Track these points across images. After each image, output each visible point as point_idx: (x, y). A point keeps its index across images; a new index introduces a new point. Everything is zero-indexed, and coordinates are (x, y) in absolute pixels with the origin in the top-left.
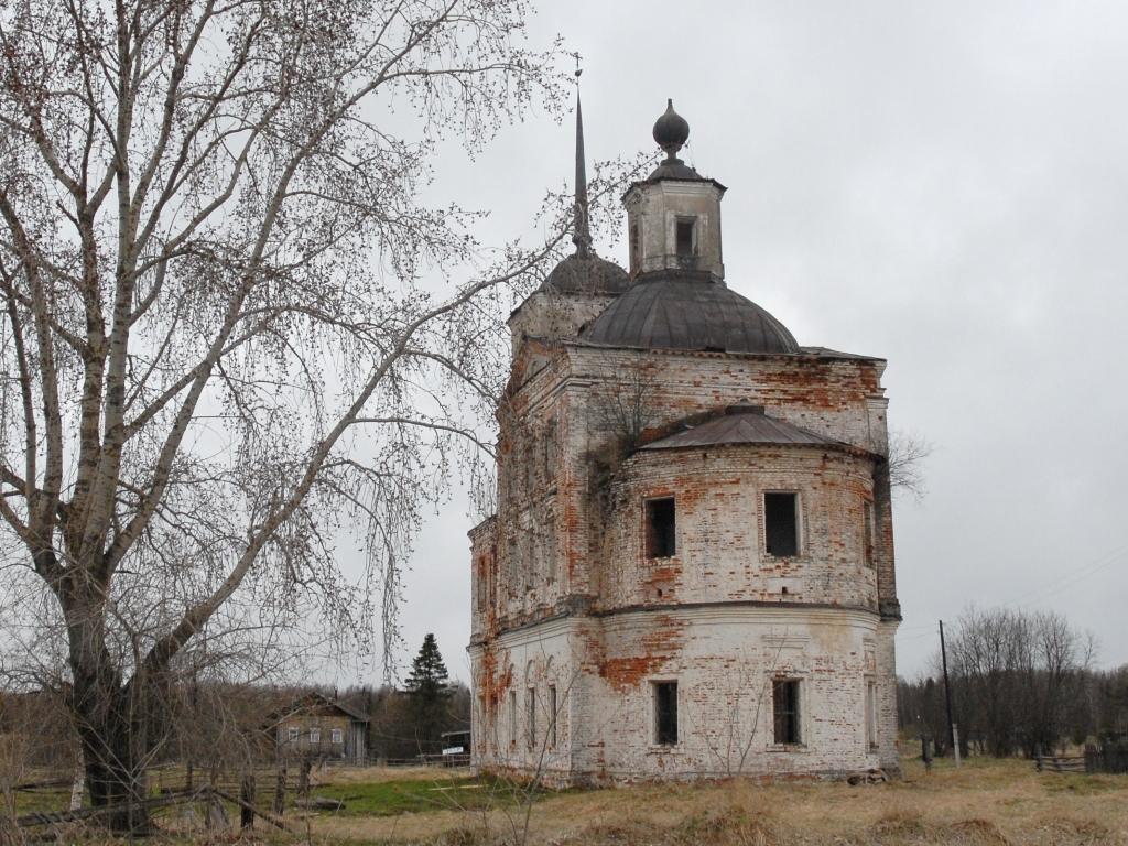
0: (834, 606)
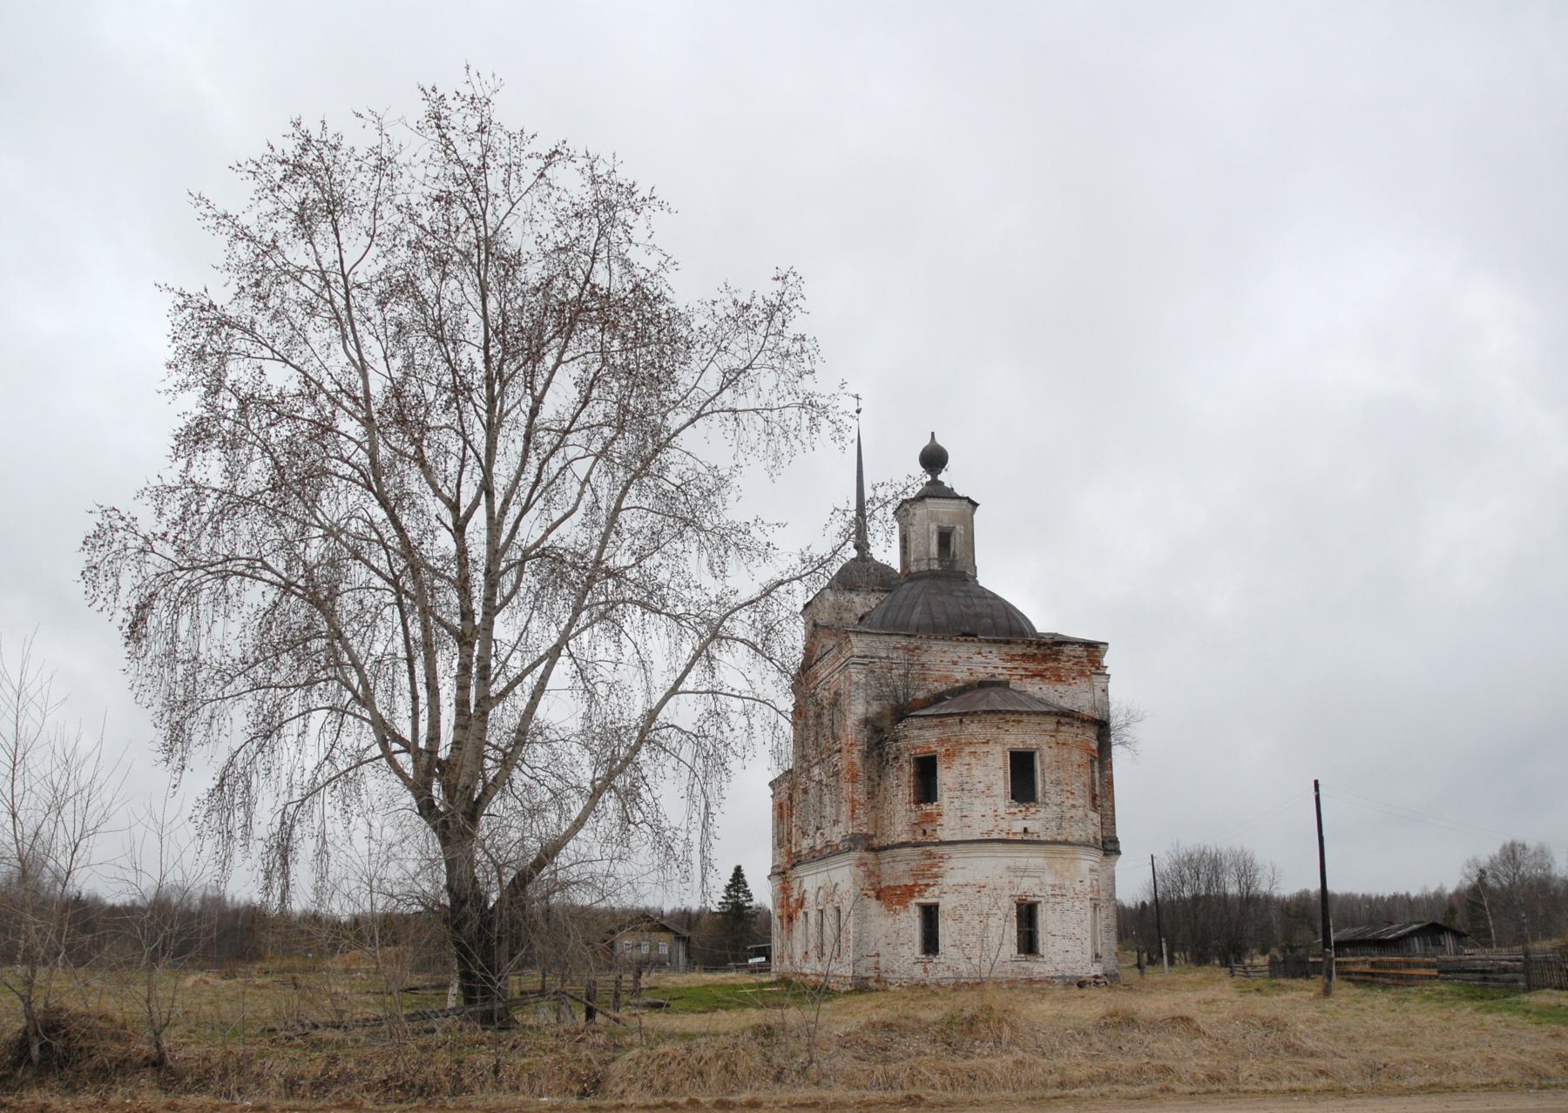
0: (1066, 843)
